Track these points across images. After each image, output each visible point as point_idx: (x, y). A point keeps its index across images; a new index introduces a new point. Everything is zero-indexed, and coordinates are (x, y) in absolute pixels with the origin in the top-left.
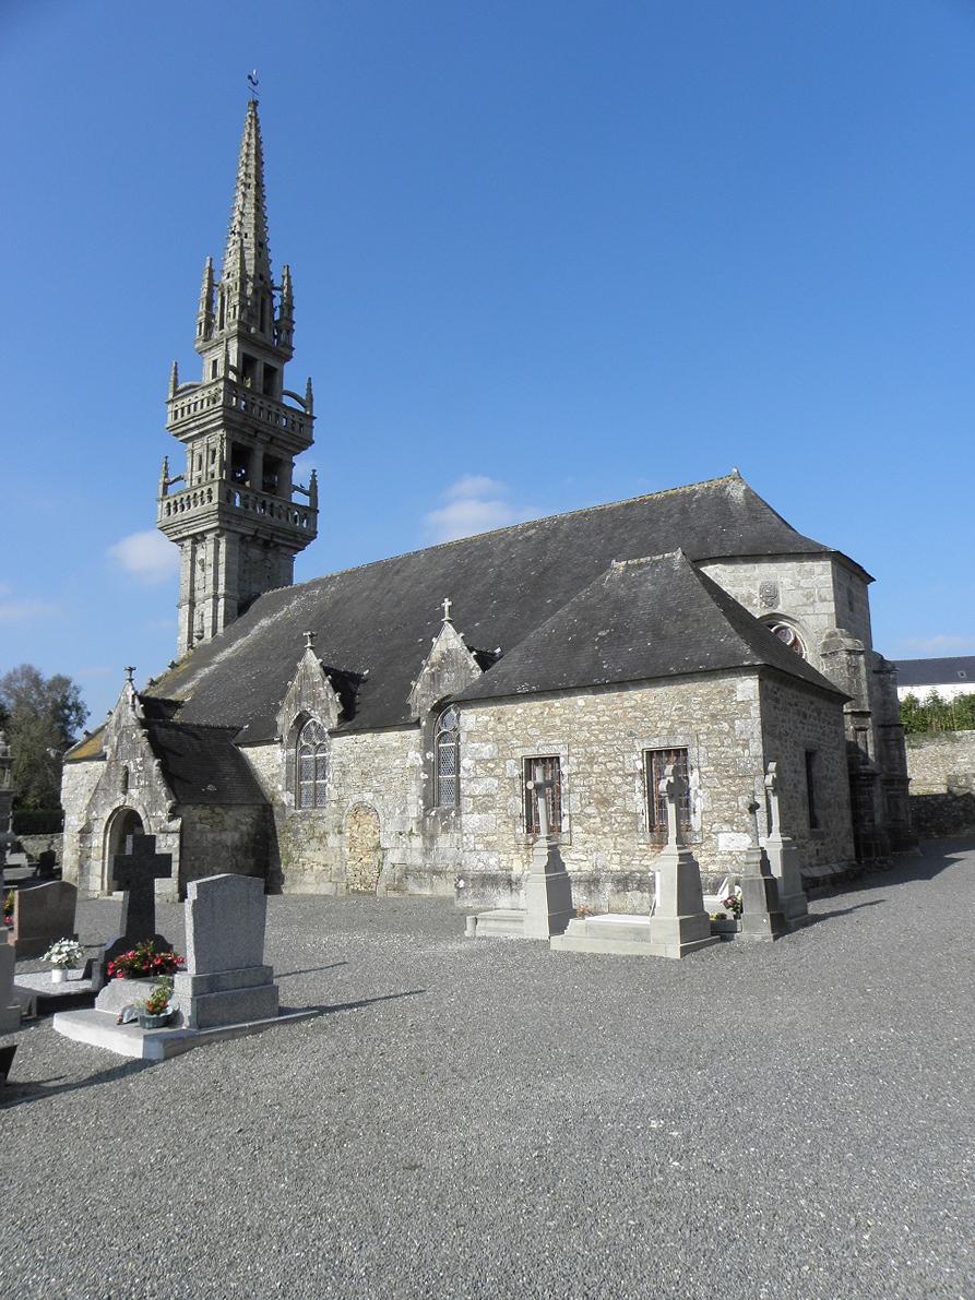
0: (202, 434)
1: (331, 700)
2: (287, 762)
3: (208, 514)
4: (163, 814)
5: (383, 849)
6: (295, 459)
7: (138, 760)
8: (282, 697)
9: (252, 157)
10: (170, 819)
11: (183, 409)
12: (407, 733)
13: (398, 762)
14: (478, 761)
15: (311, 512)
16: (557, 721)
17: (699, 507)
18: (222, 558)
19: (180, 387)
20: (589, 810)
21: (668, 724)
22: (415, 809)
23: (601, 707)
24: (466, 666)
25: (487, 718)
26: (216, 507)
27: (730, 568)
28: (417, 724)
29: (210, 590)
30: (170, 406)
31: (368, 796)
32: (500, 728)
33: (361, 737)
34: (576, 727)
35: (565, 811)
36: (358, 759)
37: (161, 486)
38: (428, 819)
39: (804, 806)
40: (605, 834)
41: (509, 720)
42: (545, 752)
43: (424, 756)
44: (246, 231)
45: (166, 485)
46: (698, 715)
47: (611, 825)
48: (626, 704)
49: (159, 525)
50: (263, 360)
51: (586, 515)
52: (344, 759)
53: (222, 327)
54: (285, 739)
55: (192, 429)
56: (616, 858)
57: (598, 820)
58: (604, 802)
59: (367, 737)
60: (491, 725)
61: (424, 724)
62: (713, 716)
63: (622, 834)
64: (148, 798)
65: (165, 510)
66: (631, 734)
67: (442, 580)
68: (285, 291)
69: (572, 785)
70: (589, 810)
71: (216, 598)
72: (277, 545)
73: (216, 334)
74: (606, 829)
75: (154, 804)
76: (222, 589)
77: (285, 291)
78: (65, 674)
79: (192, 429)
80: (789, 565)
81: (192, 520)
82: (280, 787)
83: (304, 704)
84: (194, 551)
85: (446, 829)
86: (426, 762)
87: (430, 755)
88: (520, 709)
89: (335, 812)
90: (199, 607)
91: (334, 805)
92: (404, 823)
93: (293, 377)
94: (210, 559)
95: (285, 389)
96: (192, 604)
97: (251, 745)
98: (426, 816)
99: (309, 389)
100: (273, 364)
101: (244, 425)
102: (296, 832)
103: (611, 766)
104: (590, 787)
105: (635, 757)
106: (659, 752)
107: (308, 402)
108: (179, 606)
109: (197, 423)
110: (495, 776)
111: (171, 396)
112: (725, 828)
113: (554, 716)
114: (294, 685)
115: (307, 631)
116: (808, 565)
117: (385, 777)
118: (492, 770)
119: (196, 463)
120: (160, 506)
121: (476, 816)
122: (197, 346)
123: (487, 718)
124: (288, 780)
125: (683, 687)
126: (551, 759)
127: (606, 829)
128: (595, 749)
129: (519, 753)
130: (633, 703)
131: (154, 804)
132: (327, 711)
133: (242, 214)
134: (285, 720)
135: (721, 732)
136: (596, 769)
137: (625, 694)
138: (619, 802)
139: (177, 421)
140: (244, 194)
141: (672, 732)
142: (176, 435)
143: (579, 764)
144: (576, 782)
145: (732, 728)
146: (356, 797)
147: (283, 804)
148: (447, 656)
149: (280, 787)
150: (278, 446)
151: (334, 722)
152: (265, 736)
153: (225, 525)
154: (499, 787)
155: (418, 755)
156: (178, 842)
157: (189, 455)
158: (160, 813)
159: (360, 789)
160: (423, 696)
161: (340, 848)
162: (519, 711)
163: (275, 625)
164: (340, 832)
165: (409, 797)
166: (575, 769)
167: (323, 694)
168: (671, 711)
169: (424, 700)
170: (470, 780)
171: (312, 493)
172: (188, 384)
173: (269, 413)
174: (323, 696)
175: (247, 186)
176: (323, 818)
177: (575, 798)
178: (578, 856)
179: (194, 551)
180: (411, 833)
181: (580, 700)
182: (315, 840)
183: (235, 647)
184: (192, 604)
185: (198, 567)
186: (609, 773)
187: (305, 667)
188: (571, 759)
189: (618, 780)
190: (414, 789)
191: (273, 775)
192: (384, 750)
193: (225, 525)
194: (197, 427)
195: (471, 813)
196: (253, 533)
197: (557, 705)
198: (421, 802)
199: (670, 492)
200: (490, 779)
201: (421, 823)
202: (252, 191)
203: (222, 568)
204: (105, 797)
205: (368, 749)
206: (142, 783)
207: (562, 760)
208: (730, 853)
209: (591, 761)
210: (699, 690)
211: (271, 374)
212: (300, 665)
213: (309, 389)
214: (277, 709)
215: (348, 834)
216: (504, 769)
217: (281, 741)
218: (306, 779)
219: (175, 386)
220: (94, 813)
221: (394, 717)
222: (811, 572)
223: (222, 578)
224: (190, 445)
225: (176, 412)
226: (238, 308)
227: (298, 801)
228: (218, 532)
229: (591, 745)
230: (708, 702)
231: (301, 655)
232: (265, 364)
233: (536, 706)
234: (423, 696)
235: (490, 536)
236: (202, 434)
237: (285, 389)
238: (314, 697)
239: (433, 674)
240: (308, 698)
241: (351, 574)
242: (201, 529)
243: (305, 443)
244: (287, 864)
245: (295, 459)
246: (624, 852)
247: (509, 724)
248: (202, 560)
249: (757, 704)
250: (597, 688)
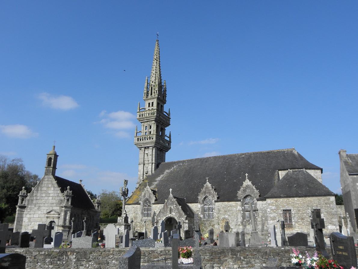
0: (148, 121)
1: (215, 194)
2: (202, 208)
3: (151, 143)
4: (184, 219)
5: (231, 228)
6: (166, 128)
7: (174, 206)
8: (200, 192)
9: (158, 53)
10: (186, 220)
11: (142, 115)
12: (237, 202)
13: (235, 209)
14: (271, 210)
15: (169, 142)
16: (290, 203)
17: (288, 155)
18: (154, 153)
19: (140, 109)
20: (299, 220)
21: (316, 204)
22: (240, 219)
23: (300, 200)
24: (253, 189)
25: (273, 201)
26: (155, 141)
27: (313, 171)
28: (240, 201)
29: (150, 161)
30: (138, 113)
31: (227, 216)
32: (276, 203)
33: (224, 203)
34: (295, 204)
35: (293, 221)
36: (223, 208)
37: (136, 133)
38: (244, 222)
39: (85, 233)
40: (303, 225)
41: (279, 202)
42: (288, 209)
43: (242, 208)
44: (157, 71)
45: (137, 133)
46: (323, 203)
47: (304, 224)
48: (306, 200)
49: (135, 143)
50: (161, 104)
51: (257, 153)
52: (219, 208)
53: (151, 94)
54: (201, 202)
55: (145, 120)
56: (306, 230)
57: (301, 222)
58: (303, 219)
59: (226, 203)
60: (274, 202)
61: (242, 201)
62: (326, 203)
63: (307, 225)
64: (178, 215)
65: (137, 140)
66: (308, 206)
67: (222, 165)
68: (165, 87)
69: (295, 215)
70: (299, 220)
71: (152, 164)
72: (163, 150)
73: (150, 96)
74: (303, 224)
75: (180, 216)
76: (154, 161)
77: (165, 87)
78: (37, 174)
79: (145, 120)
80: (313, 170)
81: (147, 143)
82: (200, 213)
83: (207, 194)
84: (145, 151)
85: (249, 224)
86: (242, 209)
87: (243, 208)
88: (281, 200)
89: (217, 219)
90: (146, 165)
91: (216, 218)
92: (237, 223)
93: (166, 108)
94: (151, 153)
95: (164, 111)
96: (144, 164)
97: (191, 203)
98: (243, 221)
99: (169, 111)
100: (162, 105)
101: (158, 120)
102: (205, 224)
103: (304, 212)
104: (299, 216)
105: (309, 210)
106: (285, 210)
107: (169, 114)
108: (139, 164)
109: (147, 119)
110: (276, 213)
111: (138, 111)
112: (330, 224)
113: (290, 202)
114: (203, 190)
115: (207, 177)
116: (316, 171)
117: (232, 212)
118: (275, 212)
119: (145, 128)
120: (135, 139)
121: (272, 221)
122: (144, 98)
123: (273, 201)
124: (202, 212)
125: (319, 198)
126: (289, 210)
127: (303, 224)
128: (300, 208)
129: (282, 209)
130: (308, 200)
131: (180, 216)
132: (214, 196)
133: (156, 67)
134: (201, 197)
135: (328, 207)
136: (300, 212)
137: (306, 198)
138: (306, 219)
139: (140, 117)
140: (156, 63)
141: (317, 206)
142: (139, 121)
143: (296, 211)
144: (296, 215)
145: (330, 206)
146: (223, 216)
147: (201, 217)
148: (247, 186)
149: (200, 213)
150: (164, 126)
151: (216, 199)
152: (195, 201)
153: (155, 145)
154: (277, 215)
155: (241, 208)
156: (188, 225)
157: (143, 126)
158: (182, 218)
159: (224, 215)
160: (241, 194)
161: (219, 228)
162: (281, 200)
163: (171, 172)
164: (219, 224)
165: (238, 217)
166: (295, 212)
167: (212, 193)
168: (317, 202)
169: (242, 195)
170: (270, 214)
171: (170, 137)
172: (142, 108)
173: (166, 119)
174: (212, 193)
175: (157, 60)
176: (213, 221)
177: (296, 218)
178: (297, 230)
179: (145, 151)
180: (239, 225)
181: (296, 199)
182: (211, 226)
183: (161, 177)
184: (144, 164)
185: (146, 155)
186: (303, 213)
187: (207, 186)
188: (294, 210)
189: (306, 215)
190: (240, 215)
191: (197, 211)
192: (231, 206)
193: (155, 145)
194: (147, 120)
195: (270, 220)
196: (159, 147)
197: (290, 199)
198: (242, 218)
199: (278, 150)
200: (274, 214)
201: (242, 223)
202: (158, 62)
203: (154, 156)
204: (163, 214)
205: (226, 206)
206: (176, 211)
207: (292, 210)
208: (331, 229)
209: (299, 211)
210: (323, 198)
211: (162, 106)
212: (205, 185)
213: (169, 111)
214: (198, 195)
215: (221, 225)
216: (278, 212)
217: (200, 203)
218: (206, 212)
219: (139, 108)
220: (159, 218)
221: (232, 198)
222: (317, 172)
223: (154, 159)
224: (143, 123)
225: (140, 115)
226: (157, 91)
227: (204, 216)
228: (153, 147)
229: (299, 207)
230: (325, 201)
231: (205, 183)
232: (161, 105)
233: (285, 199)
234: (241, 194)
235: (235, 156)
236: (148, 121)
237: (164, 111)
238: (210, 193)
239: (244, 190)
240: (208, 193)
241: (191, 160)
242: (149, 146)
243: (168, 124)
244: (202, 232)
245: (166, 128)
246: (308, 229)
247: (279, 202)
248: (147, 154)
249: (335, 202)
250: (300, 197)
